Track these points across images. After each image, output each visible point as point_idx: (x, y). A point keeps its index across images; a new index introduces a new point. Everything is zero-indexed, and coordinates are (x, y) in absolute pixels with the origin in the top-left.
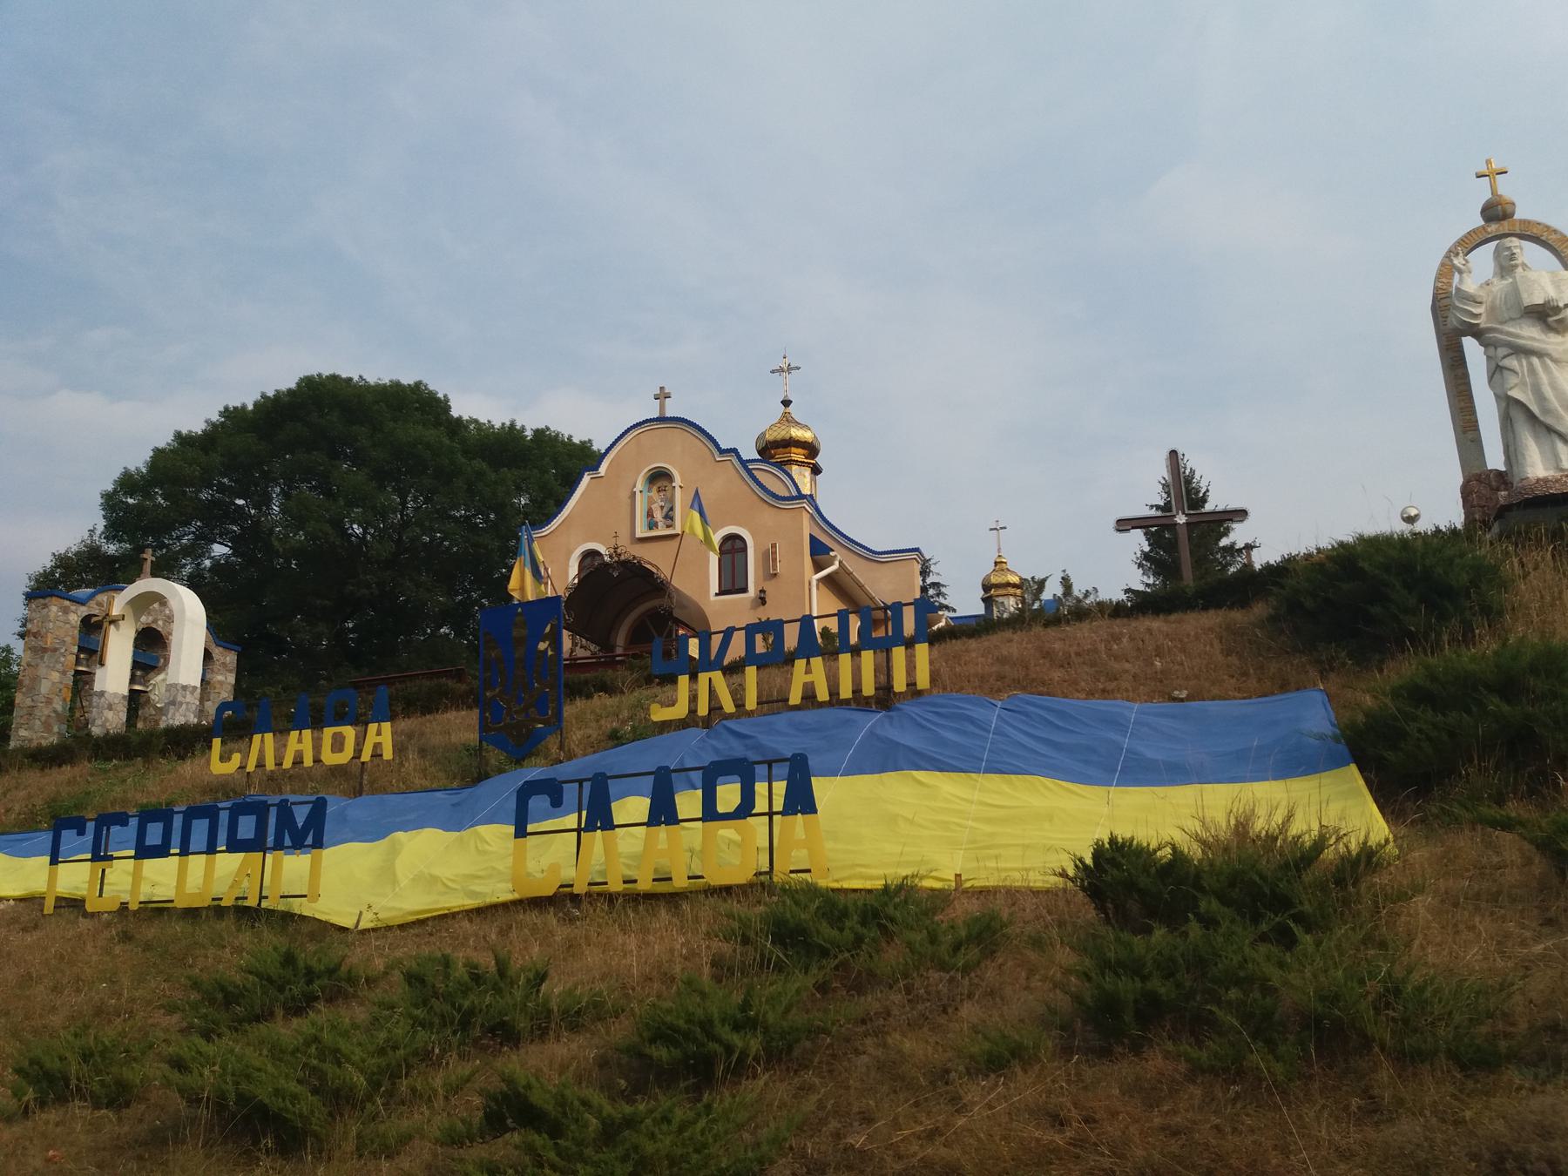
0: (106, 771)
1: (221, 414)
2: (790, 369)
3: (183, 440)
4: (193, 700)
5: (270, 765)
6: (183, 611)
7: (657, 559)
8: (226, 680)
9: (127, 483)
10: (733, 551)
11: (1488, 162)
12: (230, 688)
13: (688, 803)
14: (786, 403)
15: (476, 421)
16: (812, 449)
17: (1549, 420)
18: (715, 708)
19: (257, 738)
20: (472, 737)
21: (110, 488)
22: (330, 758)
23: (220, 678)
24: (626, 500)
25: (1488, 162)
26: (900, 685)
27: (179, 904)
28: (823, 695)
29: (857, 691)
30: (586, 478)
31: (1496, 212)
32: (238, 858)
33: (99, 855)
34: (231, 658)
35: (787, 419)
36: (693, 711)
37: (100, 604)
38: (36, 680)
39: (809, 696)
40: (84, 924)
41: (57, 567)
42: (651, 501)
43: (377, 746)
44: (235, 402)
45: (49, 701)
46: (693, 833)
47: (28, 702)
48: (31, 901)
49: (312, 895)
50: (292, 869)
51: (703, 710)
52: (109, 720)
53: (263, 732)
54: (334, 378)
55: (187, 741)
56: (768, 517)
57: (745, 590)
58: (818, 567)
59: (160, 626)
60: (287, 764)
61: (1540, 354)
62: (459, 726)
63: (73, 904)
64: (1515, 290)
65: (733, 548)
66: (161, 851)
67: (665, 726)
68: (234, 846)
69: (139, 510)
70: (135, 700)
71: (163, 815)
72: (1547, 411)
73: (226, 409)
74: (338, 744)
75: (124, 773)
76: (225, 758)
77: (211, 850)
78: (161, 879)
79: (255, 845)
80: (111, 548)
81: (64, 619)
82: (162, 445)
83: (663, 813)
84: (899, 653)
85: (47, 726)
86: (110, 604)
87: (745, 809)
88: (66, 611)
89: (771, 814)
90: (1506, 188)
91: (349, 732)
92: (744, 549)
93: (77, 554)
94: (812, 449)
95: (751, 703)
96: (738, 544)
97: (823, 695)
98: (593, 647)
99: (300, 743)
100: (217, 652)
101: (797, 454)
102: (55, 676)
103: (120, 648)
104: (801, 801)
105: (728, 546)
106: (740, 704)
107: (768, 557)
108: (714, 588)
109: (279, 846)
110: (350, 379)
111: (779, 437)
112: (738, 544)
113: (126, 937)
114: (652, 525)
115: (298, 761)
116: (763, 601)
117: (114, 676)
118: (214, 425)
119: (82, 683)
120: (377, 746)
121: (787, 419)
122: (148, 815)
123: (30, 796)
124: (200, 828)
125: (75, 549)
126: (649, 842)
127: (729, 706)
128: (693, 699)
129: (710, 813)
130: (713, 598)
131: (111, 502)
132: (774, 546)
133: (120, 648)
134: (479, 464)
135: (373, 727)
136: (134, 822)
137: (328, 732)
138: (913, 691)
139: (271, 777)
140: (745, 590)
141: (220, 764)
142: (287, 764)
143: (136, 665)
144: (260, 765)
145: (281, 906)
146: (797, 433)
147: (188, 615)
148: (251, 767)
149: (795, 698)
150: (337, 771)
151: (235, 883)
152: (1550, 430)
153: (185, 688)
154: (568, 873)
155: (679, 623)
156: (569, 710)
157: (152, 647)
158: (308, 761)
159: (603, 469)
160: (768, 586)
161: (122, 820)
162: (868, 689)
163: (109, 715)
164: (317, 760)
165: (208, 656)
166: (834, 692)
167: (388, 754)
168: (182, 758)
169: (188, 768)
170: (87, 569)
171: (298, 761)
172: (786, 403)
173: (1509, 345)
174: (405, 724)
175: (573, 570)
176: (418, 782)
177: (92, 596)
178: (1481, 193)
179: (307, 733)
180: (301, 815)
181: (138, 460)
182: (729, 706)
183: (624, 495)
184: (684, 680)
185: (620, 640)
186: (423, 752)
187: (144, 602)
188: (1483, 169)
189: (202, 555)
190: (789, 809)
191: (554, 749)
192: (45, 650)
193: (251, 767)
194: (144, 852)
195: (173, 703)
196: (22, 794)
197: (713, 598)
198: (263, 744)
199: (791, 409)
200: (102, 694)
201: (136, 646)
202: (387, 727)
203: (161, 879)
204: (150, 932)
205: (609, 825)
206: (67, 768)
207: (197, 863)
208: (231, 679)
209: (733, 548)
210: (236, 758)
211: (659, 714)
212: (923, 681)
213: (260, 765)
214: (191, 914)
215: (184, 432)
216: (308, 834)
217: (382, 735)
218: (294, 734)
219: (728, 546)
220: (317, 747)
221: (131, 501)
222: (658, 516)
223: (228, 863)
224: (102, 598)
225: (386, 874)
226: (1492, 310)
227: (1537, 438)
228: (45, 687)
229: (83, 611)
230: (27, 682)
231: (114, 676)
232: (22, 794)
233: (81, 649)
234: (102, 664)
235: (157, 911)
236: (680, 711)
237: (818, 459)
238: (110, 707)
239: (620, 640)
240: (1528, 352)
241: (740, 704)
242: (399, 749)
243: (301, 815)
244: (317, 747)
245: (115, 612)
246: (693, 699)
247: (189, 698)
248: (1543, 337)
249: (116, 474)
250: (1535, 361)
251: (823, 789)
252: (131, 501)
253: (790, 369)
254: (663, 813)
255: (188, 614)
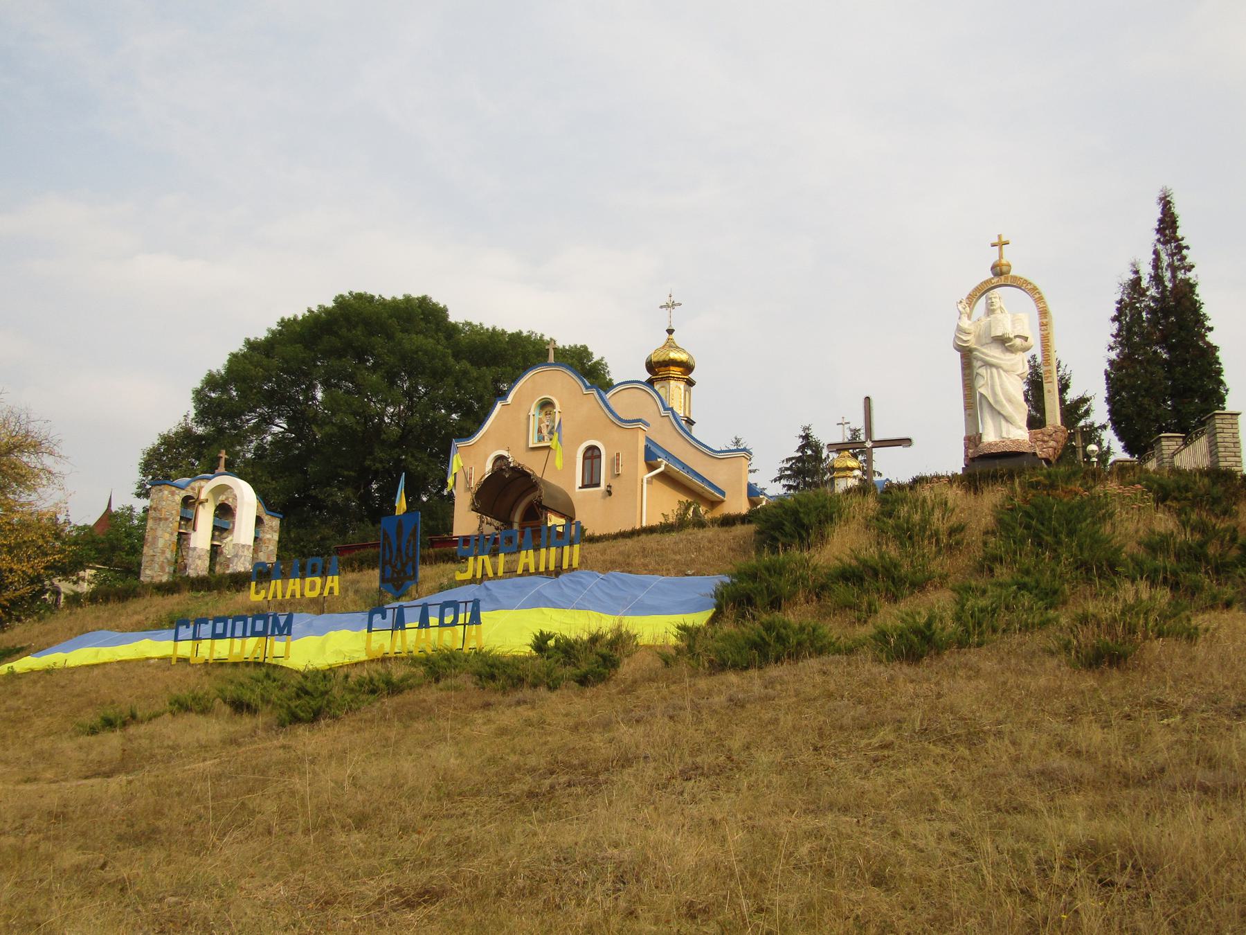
0: (197, 598)
1: (279, 324)
2: (667, 306)
3: (252, 346)
4: (248, 554)
5: (279, 597)
6: (243, 498)
7: (533, 464)
8: (272, 536)
9: (212, 382)
10: (592, 458)
11: (999, 237)
12: (275, 543)
13: (434, 620)
14: (670, 331)
15: (470, 324)
16: (687, 367)
17: (998, 408)
18: (484, 575)
19: (273, 582)
20: (377, 584)
21: (199, 386)
22: (309, 594)
23: (269, 536)
24: (524, 420)
25: (999, 237)
26: (565, 566)
27: (231, 660)
28: (532, 570)
29: (547, 568)
30: (499, 405)
31: (999, 270)
32: (254, 640)
33: (196, 638)
34: (276, 523)
35: (670, 345)
36: (474, 576)
37: (193, 489)
38: (155, 538)
39: (526, 570)
40: (189, 669)
41: (162, 444)
42: (541, 421)
43: (331, 589)
44: (289, 315)
45: (163, 552)
46: (434, 633)
47: (151, 553)
48: (165, 659)
49: (286, 657)
50: (277, 647)
51: (479, 576)
52: (198, 566)
53: (276, 579)
54: (360, 297)
55: (239, 582)
56: (616, 434)
57: (598, 485)
58: (651, 467)
59: (230, 502)
60: (288, 596)
61: (997, 367)
62: (371, 578)
63: (184, 661)
64: (989, 326)
65: (592, 454)
66: (222, 636)
67: (463, 583)
68: (254, 634)
69: (219, 403)
70: (215, 551)
71: (223, 620)
72: (997, 402)
73: (283, 320)
74: (312, 588)
75: (207, 599)
76: (257, 592)
77: (244, 636)
78: (223, 649)
79: (263, 634)
80: (200, 430)
81: (170, 499)
82: (235, 350)
83: (424, 623)
84: (567, 548)
85: (162, 568)
86: (201, 488)
87: (455, 623)
88: (173, 494)
89: (465, 625)
90: (1009, 256)
91: (318, 580)
92: (600, 457)
93: (177, 433)
94: (687, 367)
95: (500, 573)
96: (596, 453)
97: (532, 570)
98: (497, 523)
99: (294, 585)
100: (266, 518)
101: (675, 371)
102: (167, 536)
103: (205, 518)
104: (475, 619)
105: (589, 454)
106: (495, 574)
107: (615, 462)
108: (579, 483)
109: (273, 634)
110: (373, 297)
111: (661, 359)
112: (596, 453)
113: (208, 674)
114: (541, 439)
115: (293, 596)
116: (610, 493)
117: (201, 538)
118: (273, 332)
119: (182, 539)
120: (331, 589)
121: (670, 345)
122: (217, 620)
123: (158, 611)
124: (240, 624)
125: (174, 430)
126: (418, 636)
127: (491, 574)
128: (475, 571)
129: (442, 624)
130: (577, 490)
131: (199, 396)
132: (618, 455)
133: (205, 518)
134: (465, 364)
135: (330, 578)
136: (211, 622)
137: (308, 580)
138: (571, 569)
139: (281, 604)
140: (598, 485)
141: (255, 596)
142: (288, 596)
143: (215, 528)
144: (275, 596)
145: (274, 662)
146: (674, 355)
147: (246, 497)
148: (270, 598)
149: (520, 572)
150: (313, 600)
151: (254, 651)
152: (999, 413)
153: (243, 546)
154: (387, 649)
155: (547, 509)
156: (424, 571)
157: (225, 512)
158: (298, 596)
159: (510, 399)
160: (615, 484)
161: (205, 621)
162: (552, 568)
163: (199, 562)
164: (302, 595)
165: (259, 521)
166: (537, 569)
167: (336, 592)
168: (238, 591)
169: (240, 597)
170: (183, 446)
171: (293, 596)
172: (670, 331)
173: (982, 360)
174: (351, 576)
175: (489, 466)
176: (351, 607)
177: (189, 483)
178: (993, 256)
179: (298, 580)
180: (282, 620)
181: (219, 365)
182: (491, 574)
183: (523, 417)
184: (471, 559)
185: (517, 518)
186: (356, 592)
187: (223, 489)
188: (996, 241)
189: (265, 432)
190: (471, 623)
191: (414, 593)
192: (160, 519)
193: (270, 598)
194: (215, 636)
195: (236, 556)
196: (154, 610)
197: (577, 490)
198: (276, 585)
199: (674, 336)
200: (195, 549)
201: (216, 516)
202: (336, 578)
203: (223, 649)
204: (218, 672)
205: (428, 626)
206: (176, 595)
207: (237, 642)
208: (276, 537)
209: (592, 454)
210: (263, 593)
211: (460, 577)
212: (575, 564)
213: (275, 596)
214: (235, 664)
215: (252, 339)
216: (284, 630)
217: (334, 582)
218: (291, 581)
219: (589, 454)
220: (302, 589)
221: (213, 395)
222: (545, 432)
223: (252, 642)
224: (196, 484)
225: (322, 649)
226: (978, 337)
227: (993, 418)
228: (161, 543)
229: (183, 494)
230: (150, 539)
231: (201, 538)
232: (154, 610)
233: (182, 518)
234: (194, 530)
235: (221, 663)
236: (468, 575)
237: (692, 376)
238: (199, 557)
239: (517, 518)
240: (991, 365)
241: (495, 574)
242: (344, 590)
243: (282, 620)
244: (302, 589)
245: (203, 497)
246: (475, 571)
247: (246, 553)
248: (1002, 356)
249: (203, 375)
250: (994, 370)
251: (483, 615)
252: (213, 395)
253: (667, 306)
254: (424, 623)
255: (246, 499)
